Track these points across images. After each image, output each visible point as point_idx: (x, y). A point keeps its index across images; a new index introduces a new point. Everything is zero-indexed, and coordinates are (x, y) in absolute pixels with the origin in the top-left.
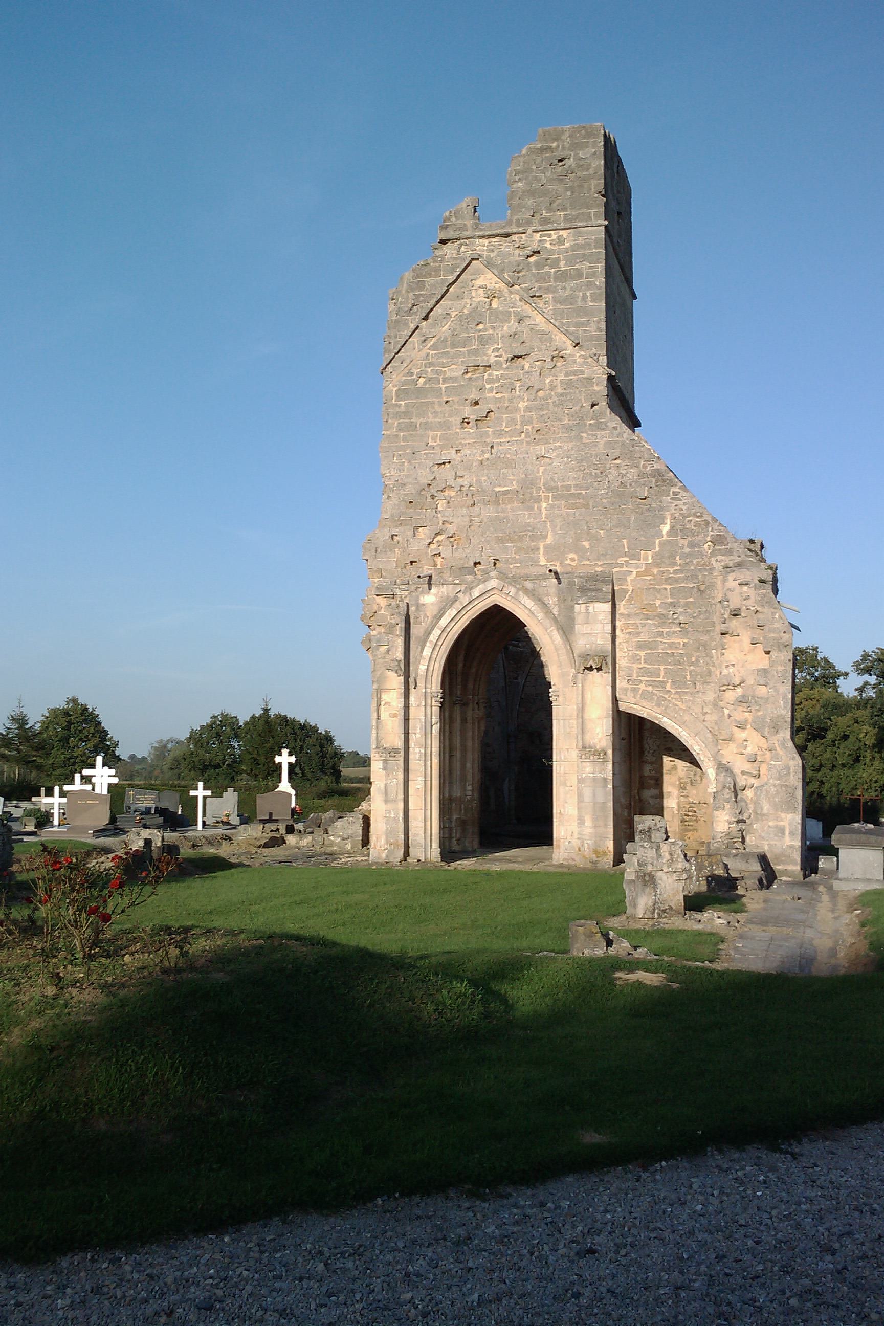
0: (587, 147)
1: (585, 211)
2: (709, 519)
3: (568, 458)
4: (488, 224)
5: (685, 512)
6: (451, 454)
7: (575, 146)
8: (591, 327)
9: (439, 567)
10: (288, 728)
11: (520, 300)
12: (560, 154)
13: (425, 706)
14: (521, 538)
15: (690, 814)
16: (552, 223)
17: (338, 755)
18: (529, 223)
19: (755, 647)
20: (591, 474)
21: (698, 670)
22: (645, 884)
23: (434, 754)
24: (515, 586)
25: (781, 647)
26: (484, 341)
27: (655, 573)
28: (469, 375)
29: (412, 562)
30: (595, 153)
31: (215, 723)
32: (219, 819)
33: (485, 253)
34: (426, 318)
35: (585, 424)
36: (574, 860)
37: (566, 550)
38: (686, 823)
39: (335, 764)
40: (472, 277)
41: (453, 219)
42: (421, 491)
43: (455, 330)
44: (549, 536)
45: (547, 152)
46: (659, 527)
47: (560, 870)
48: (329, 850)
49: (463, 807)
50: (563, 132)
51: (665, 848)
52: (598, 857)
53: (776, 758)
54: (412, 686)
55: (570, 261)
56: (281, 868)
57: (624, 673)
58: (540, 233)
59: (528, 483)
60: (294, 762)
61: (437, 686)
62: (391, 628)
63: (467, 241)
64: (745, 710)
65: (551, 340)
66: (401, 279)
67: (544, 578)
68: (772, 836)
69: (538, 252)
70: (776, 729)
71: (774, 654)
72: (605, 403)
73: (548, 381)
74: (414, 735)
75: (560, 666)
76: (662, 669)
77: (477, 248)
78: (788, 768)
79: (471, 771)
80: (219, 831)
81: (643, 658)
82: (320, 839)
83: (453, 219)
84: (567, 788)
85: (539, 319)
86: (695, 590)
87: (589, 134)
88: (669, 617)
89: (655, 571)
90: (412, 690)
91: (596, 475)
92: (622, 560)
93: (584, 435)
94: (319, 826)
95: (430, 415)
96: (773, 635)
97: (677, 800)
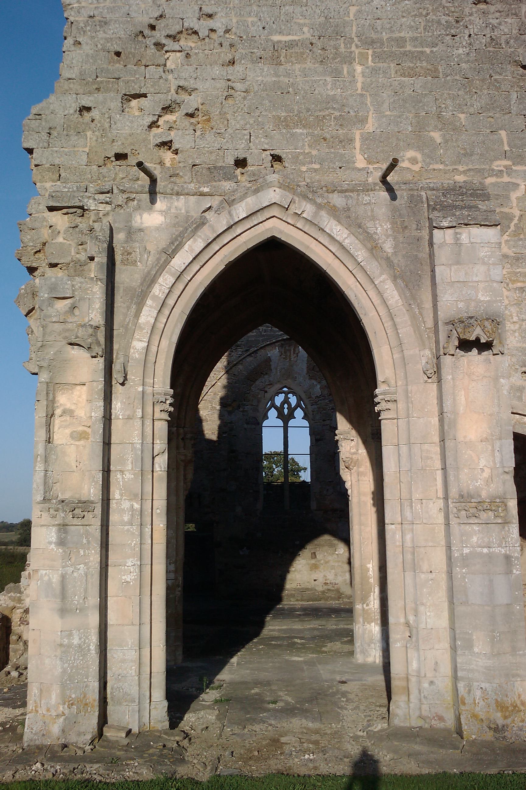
14: (320, 120)
23: (157, 511)
24: (312, 201)
36: (441, 719)
44: (370, 120)
52: (506, 718)
54: (117, 376)
61: (164, 383)
90: (117, 389)
91: (448, 25)
92: (500, 164)
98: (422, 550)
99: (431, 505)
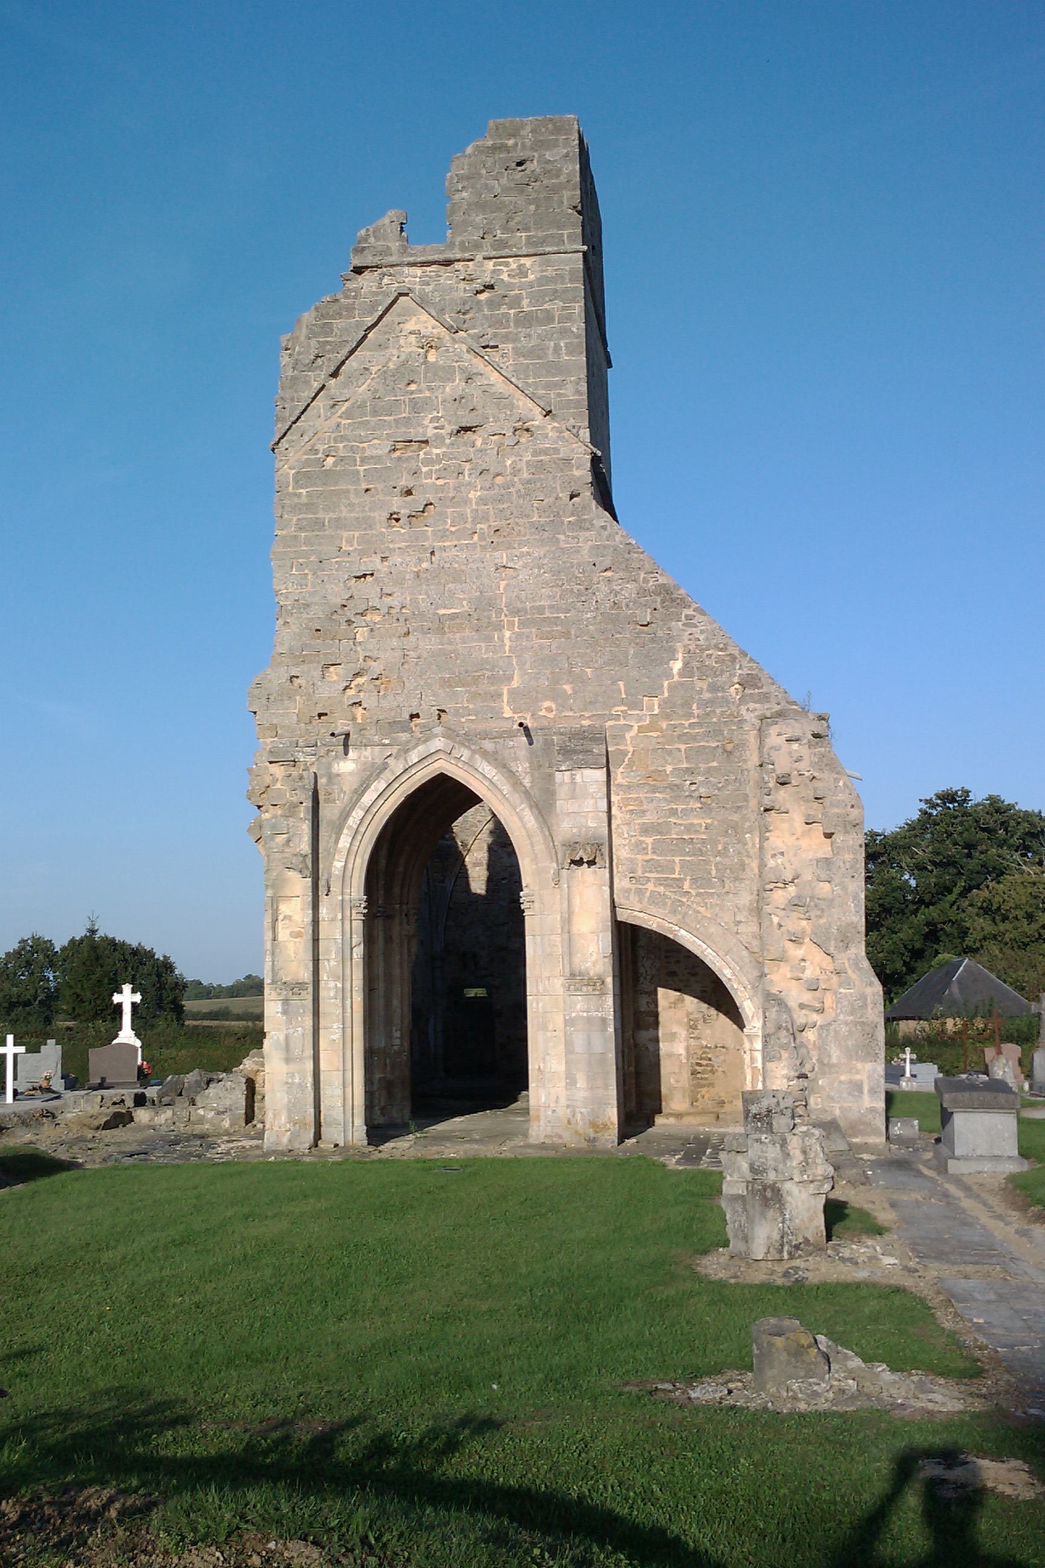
0: (556, 146)
1: (555, 231)
2: (736, 653)
3: (539, 568)
4: (420, 247)
5: (702, 642)
6: (373, 563)
7: (540, 145)
8: (566, 389)
9: (359, 721)
10: (116, 953)
11: (468, 352)
12: (520, 155)
13: (342, 919)
14: (476, 680)
15: (704, 1062)
16: (510, 247)
17: (181, 986)
18: (477, 247)
19: (811, 828)
20: (572, 591)
21: (727, 861)
22: (766, 1203)
24: (469, 748)
25: (848, 827)
26: (417, 407)
27: (664, 727)
28: (398, 453)
29: (320, 715)
30: (567, 155)
31: (24, 949)
32: (37, 1085)
33: (418, 287)
34: (335, 374)
35: (563, 522)
36: (560, 1137)
37: (540, 696)
38: (699, 1076)
39: (176, 998)
40: (398, 320)
41: (372, 240)
42: (332, 614)
43: (376, 391)
44: (516, 677)
45: (501, 152)
46: (667, 663)
47: (544, 1154)
48: (198, 1129)
49: (388, 1061)
50: (523, 126)
51: (794, 1143)
52: (596, 1132)
53: (848, 984)
54: (322, 891)
55: (537, 298)
56: (134, 1166)
57: (624, 868)
58: (494, 260)
59: (485, 603)
60: (139, 1002)
61: (359, 892)
62: (292, 809)
63: (392, 270)
64: (802, 916)
65: (512, 406)
66: (299, 321)
67: (511, 735)
68: (844, 1095)
69: (491, 287)
70: (845, 943)
71: (839, 838)
72: (589, 494)
73: (509, 462)
74: (326, 963)
75: (535, 859)
76: (677, 862)
77: (406, 280)
78: (863, 997)
79: (399, 1011)
80: (37, 1104)
81: (650, 847)
82: (185, 1114)
83: (372, 240)
84: (549, 1034)
85: (494, 378)
86: (720, 750)
87: (558, 130)
88: (685, 788)
89: (664, 725)
93: (562, 537)
94: (180, 1095)
95: (343, 508)
96: (836, 810)
97: (685, 1044)
98: (549, 1015)
99: (556, 981)
